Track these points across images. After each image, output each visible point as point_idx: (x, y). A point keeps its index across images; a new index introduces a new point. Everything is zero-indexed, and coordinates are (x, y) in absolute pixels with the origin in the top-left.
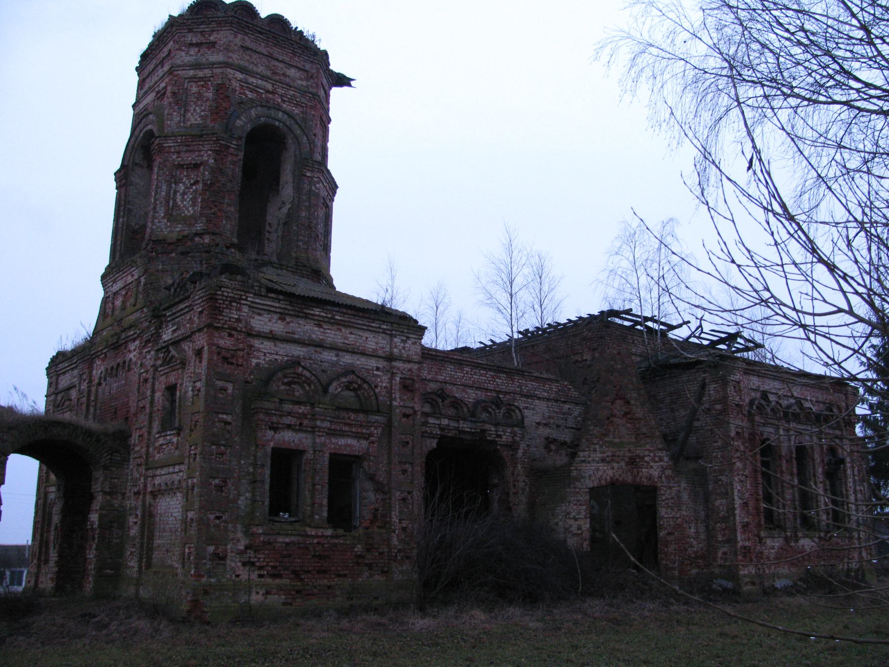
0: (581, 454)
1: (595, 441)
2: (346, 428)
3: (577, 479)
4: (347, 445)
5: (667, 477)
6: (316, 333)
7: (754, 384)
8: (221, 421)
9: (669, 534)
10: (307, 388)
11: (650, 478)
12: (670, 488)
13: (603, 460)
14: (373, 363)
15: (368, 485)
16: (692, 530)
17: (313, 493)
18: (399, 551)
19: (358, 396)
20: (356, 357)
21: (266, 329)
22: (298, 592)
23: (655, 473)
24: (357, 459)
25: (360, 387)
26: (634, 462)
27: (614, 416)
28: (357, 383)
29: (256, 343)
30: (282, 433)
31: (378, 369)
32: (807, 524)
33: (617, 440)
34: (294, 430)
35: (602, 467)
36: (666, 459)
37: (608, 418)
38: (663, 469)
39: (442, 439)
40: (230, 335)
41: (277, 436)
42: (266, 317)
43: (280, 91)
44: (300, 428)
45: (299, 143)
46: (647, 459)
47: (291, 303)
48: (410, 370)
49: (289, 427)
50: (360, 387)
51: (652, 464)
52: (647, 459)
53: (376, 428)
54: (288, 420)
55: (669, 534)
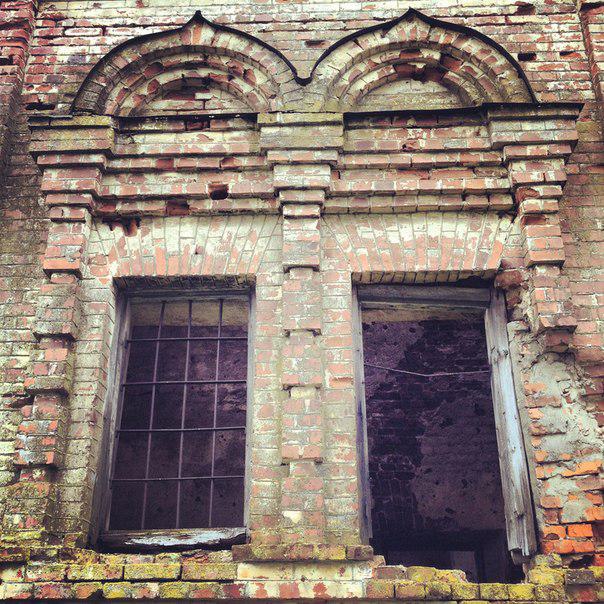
2: (411, 183)
10: (246, 88)
15: (552, 380)
24: (490, 289)
25: (449, 55)
28: (430, 44)
30: (156, 232)
44: (221, 206)
45: (382, 214)
49: (178, 206)
50: (449, 55)
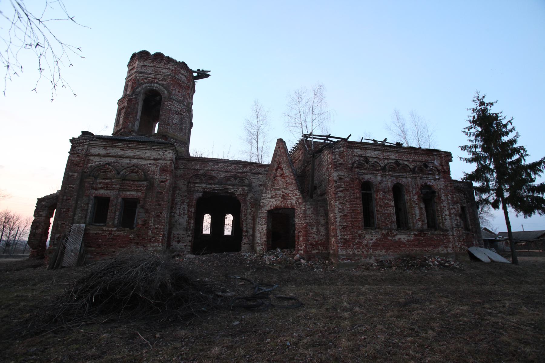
0: (263, 195)
1: (269, 188)
2: (129, 188)
3: (262, 207)
4: (130, 195)
5: (299, 204)
6: (121, 153)
7: (357, 153)
8: (71, 187)
9: (299, 232)
11: (291, 204)
12: (301, 208)
13: (272, 197)
14: (148, 162)
16: (314, 230)
17: (114, 214)
18: (153, 237)
19: (138, 175)
20: (139, 160)
21: (97, 153)
22: (98, 253)
23: (294, 202)
26: (285, 197)
27: (277, 176)
29: (92, 158)
31: (150, 164)
32: (402, 223)
33: (278, 187)
34: (105, 190)
35: (272, 200)
36: (298, 194)
37: (274, 178)
38: (298, 199)
39: (205, 193)
40: (78, 156)
41: (96, 192)
42: (97, 149)
43: (158, 77)
44: (107, 189)
46: (290, 195)
47: (107, 142)
48: (166, 163)
49: (102, 188)
51: (292, 197)
52: (290, 195)
53: (143, 187)
54: (99, 186)
55: (299, 232)
